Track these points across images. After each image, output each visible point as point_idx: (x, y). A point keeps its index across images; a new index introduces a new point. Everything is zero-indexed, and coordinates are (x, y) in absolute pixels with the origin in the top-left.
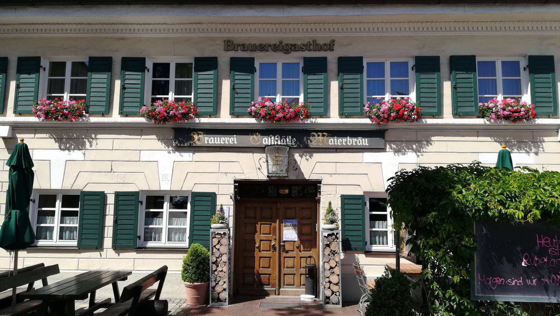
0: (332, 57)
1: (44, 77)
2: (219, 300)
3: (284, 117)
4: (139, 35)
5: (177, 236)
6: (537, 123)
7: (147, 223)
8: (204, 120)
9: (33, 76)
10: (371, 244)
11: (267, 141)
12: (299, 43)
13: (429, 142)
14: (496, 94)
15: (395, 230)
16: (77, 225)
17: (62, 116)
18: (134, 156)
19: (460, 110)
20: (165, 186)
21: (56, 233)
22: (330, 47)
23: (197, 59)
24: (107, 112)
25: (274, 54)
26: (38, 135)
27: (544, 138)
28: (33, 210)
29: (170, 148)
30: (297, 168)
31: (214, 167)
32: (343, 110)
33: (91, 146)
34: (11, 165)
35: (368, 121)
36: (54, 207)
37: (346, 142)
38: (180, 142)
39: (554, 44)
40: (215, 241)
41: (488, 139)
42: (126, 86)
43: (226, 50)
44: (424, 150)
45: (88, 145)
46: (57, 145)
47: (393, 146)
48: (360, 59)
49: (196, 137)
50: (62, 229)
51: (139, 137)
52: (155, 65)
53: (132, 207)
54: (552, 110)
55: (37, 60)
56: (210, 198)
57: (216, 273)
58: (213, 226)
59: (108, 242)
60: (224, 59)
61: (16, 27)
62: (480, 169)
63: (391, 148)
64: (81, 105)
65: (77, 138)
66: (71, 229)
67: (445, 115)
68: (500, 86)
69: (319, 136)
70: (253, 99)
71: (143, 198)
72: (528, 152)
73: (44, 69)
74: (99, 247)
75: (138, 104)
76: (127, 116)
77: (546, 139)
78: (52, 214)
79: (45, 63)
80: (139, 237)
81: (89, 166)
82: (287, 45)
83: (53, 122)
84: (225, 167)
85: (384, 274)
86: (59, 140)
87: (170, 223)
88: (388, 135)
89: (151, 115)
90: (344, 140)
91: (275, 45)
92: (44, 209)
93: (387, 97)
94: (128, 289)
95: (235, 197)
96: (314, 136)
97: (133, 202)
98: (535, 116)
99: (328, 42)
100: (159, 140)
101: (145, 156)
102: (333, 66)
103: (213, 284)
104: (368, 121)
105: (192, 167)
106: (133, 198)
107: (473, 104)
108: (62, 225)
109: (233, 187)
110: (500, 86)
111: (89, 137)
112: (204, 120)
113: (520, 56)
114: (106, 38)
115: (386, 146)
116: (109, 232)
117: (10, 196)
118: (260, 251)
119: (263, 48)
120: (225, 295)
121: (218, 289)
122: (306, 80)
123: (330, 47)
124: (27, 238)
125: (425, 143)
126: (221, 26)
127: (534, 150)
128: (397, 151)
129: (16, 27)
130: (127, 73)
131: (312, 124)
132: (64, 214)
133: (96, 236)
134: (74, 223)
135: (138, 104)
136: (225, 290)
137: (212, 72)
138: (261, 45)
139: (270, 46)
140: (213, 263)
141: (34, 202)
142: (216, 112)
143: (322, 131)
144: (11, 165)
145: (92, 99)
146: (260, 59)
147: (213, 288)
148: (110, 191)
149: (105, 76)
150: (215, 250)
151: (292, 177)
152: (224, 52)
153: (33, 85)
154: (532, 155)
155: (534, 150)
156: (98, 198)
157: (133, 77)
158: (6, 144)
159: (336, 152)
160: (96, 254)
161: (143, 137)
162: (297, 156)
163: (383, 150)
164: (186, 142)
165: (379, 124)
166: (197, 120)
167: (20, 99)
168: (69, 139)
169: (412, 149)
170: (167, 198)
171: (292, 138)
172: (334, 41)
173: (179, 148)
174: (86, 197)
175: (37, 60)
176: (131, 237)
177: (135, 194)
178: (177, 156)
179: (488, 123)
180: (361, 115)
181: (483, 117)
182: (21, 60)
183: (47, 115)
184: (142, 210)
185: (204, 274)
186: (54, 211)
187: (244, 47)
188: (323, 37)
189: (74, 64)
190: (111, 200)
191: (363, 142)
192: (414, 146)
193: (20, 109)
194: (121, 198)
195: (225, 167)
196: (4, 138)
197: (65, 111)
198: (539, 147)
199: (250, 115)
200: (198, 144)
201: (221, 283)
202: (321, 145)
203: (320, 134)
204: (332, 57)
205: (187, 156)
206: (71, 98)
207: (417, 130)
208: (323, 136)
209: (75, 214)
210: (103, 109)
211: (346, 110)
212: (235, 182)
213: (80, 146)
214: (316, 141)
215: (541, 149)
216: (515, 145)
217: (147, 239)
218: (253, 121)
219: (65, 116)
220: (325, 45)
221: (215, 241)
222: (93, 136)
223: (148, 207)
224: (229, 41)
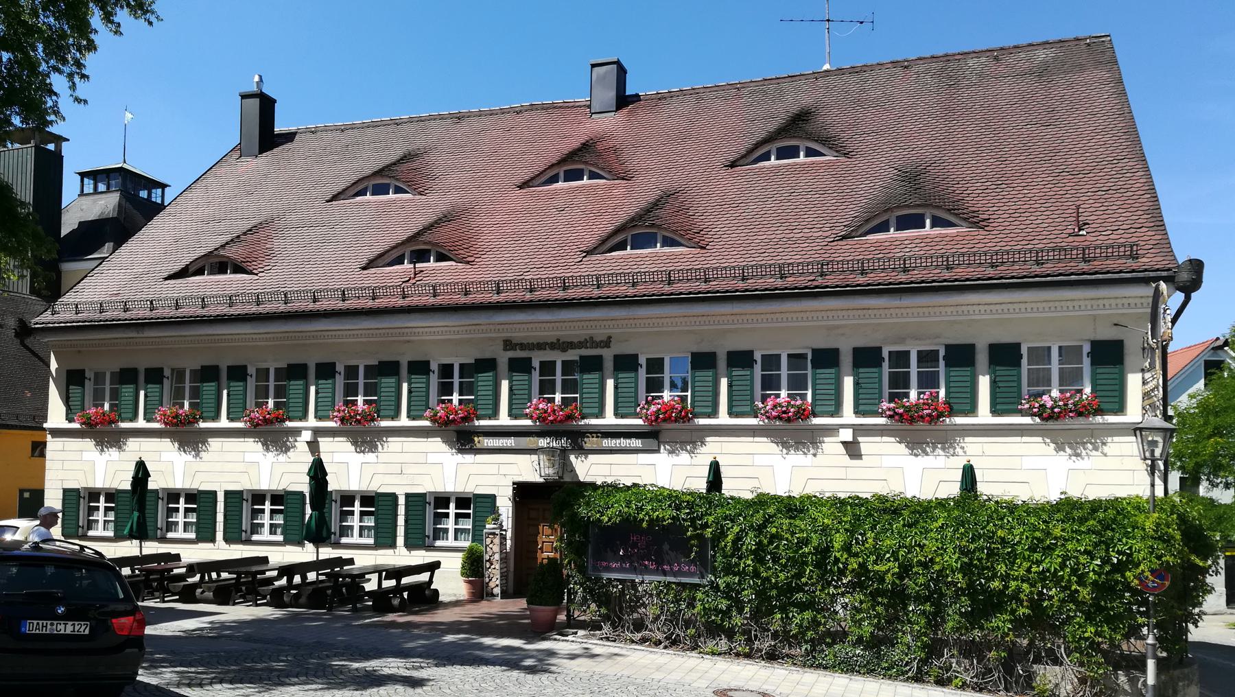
0: (608, 355)
1: (340, 381)
2: (493, 595)
3: (555, 420)
4: (423, 338)
5: (463, 536)
6: (813, 423)
7: (435, 524)
8: (483, 423)
9: (330, 381)
10: (167, 531)
11: (543, 442)
12: (576, 340)
13: (703, 443)
14: (909, 388)
16: (470, 527)
17: (355, 422)
18: (421, 459)
19: (861, 408)
20: (99, 484)
21: (451, 534)
22: (607, 343)
23: (816, 352)
24: (134, 417)
25: (552, 352)
26: (336, 439)
27: (825, 439)
28: (335, 510)
29: (454, 450)
30: (573, 470)
31: (494, 469)
32: (858, 408)
33: (383, 449)
35: (640, 422)
36: (179, 503)
37: (620, 444)
38: (462, 445)
39: (843, 334)
40: (489, 540)
41: (765, 439)
42: (412, 390)
43: (505, 349)
44: (698, 451)
45: (380, 446)
46: (907, 451)
47: (667, 447)
48: (1017, 346)
49: (476, 439)
50: (361, 528)
51: (425, 440)
52: (258, 370)
53: (420, 508)
54: (832, 408)
55: (332, 366)
56: (490, 500)
57: (490, 570)
58: (488, 526)
59: (400, 540)
60: (503, 358)
61: (313, 334)
63: (665, 449)
64: (373, 408)
65: (371, 442)
66: (369, 528)
67: (720, 415)
68: (784, 381)
69: (593, 437)
70: (530, 401)
71: (430, 499)
72: (805, 454)
73: (434, 372)
74: (213, 540)
75: (241, 410)
76: (622, 417)
77: (826, 439)
78: (352, 513)
79: (340, 368)
80: (428, 537)
81: (381, 468)
82: (564, 343)
83: (348, 427)
84: (504, 469)
85: (1206, 597)
86: (355, 443)
87: (271, 519)
88: (662, 437)
89: (433, 419)
90: (618, 441)
91: (552, 343)
92: (439, 511)
93: (558, 397)
95: (514, 499)
96: (588, 437)
97: (421, 503)
98: (696, 416)
99: (604, 338)
101: (432, 458)
102: (609, 365)
103: (487, 580)
104: (640, 422)
105: (474, 469)
106: (238, 496)
107: (749, 403)
108: (272, 522)
109: (511, 488)
110: (784, 381)
111: (380, 440)
112: (483, 423)
113: (1082, 340)
114: (394, 341)
115: (659, 447)
116: (401, 531)
118: (542, 552)
119: (540, 346)
120: (497, 591)
121: (492, 584)
122: (814, 375)
123: (607, 343)
124: (325, 534)
125: (699, 443)
126: (499, 327)
127: (812, 451)
128: (671, 452)
129: (313, 334)
130: (514, 374)
131: (586, 425)
132: (458, 516)
133: (390, 535)
134: (279, 520)
135: (424, 408)
136: (497, 586)
137: (491, 374)
138: (538, 344)
140: (487, 561)
141: (430, 504)
142: (495, 414)
143: (596, 433)
145: (479, 402)
146: (537, 359)
147: (488, 583)
148: (401, 492)
149: (393, 380)
150: (488, 549)
151: (567, 479)
153: (158, 394)
154: (810, 456)
155: (812, 451)
156: (390, 498)
157: (419, 380)
158: (846, 449)
159: (611, 454)
160: (390, 551)
161: (429, 439)
162: (572, 458)
163: (658, 451)
164: (468, 444)
165: (651, 425)
166: (477, 423)
167: (319, 404)
168: (364, 442)
169: (686, 450)
170: (183, 495)
171: (567, 439)
173: (461, 451)
174: (478, 500)
175: (332, 366)
176: (237, 530)
177: (423, 496)
178: (361, 457)
179: (761, 423)
180: (636, 416)
181: (756, 417)
182: (318, 366)
183: (342, 420)
184: (430, 511)
185: (478, 571)
186: (448, 513)
187: (523, 347)
188: (600, 333)
189: (366, 367)
190: (402, 501)
191: (636, 443)
192: (688, 448)
193: (319, 413)
195: (504, 469)
196: (307, 442)
197: (358, 417)
198: (818, 448)
199: (526, 416)
200: (479, 446)
201: (494, 580)
202: (595, 447)
203: (595, 435)
204: (608, 355)
205: (469, 458)
206: (366, 402)
207: (691, 430)
208: (597, 437)
209: (467, 516)
210: (392, 413)
211: (621, 411)
212: (514, 484)
213: (373, 448)
214: (590, 443)
215: (820, 450)
216: (792, 446)
217: (436, 538)
218: (528, 422)
219: (358, 422)
220: (602, 341)
221: (489, 540)
222: (384, 439)
223: (436, 508)
224: (507, 341)
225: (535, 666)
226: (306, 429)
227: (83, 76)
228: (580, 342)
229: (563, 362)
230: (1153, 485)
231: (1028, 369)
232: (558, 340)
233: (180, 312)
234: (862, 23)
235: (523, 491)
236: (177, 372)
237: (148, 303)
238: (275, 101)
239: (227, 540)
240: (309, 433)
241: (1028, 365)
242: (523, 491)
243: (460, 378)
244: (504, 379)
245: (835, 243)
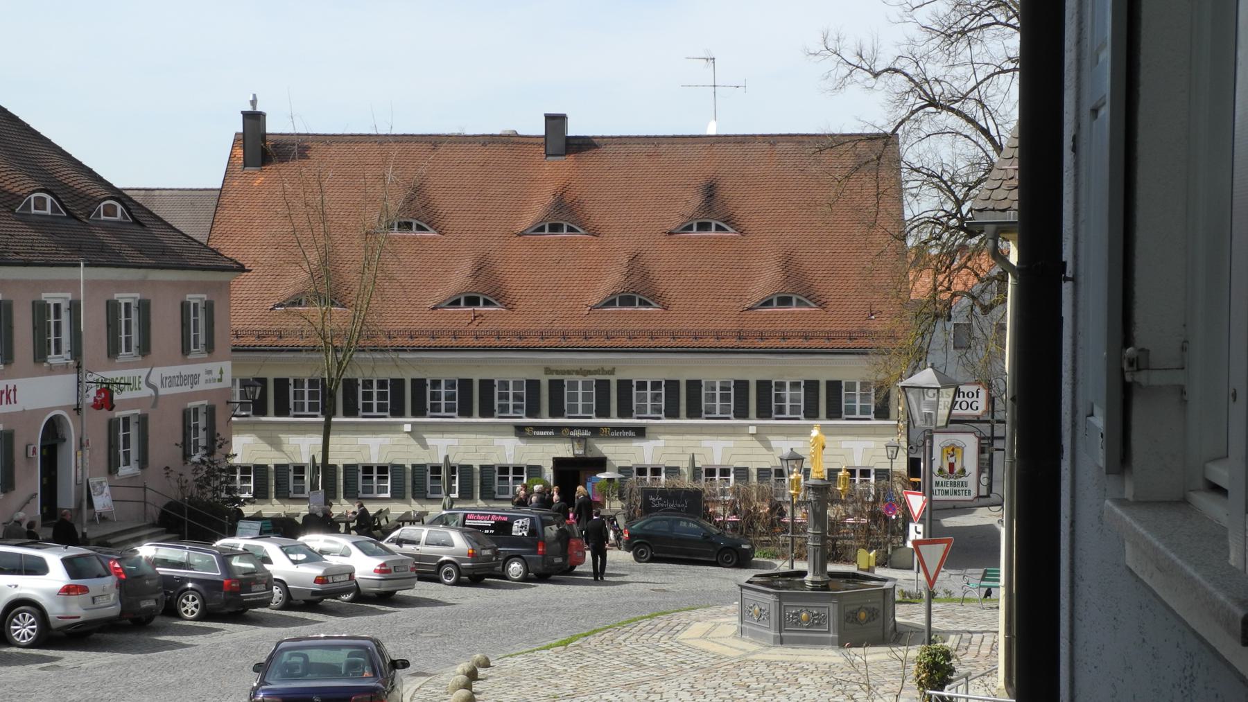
12: (593, 369)
15: (525, 535)
34: (343, 377)
43: (546, 374)
62: (145, 581)
82: (585, 370)
94: (362, 593)
99: (610, 369)
100: (269, 571)
117: (158, 532)
123: (612, 372)
139: (574, 371)
144: (343, 377)
148: (476, 465)
152: (545, 376)
172: (614, 369)
187: (558, 372)
188: (608, 367)
194: (879, 473)
220: (609, 371)
224: (547, 368)
225: (386, 663)
228: (595, 371)
229: (583, 382)
230: (931, 90)
232: (581, 369)
234: (738, 87)
235: (558, 462)
240: (410, 426)
242: (558, 462)
243: (304, 403)
244: (4, 426)
245: (744, 313)
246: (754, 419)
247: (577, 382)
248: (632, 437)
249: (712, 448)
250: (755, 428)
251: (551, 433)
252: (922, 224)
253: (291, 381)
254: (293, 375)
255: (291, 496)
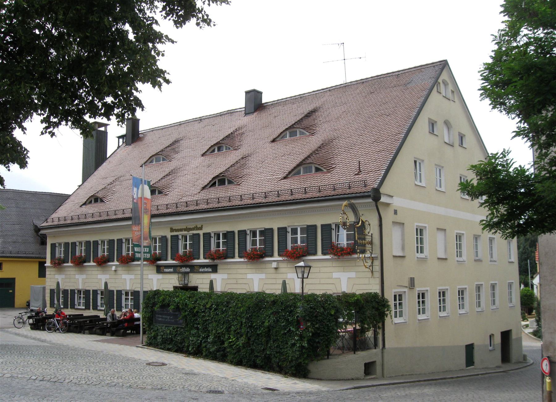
123: (201, 228)
139: (183, 229)
152: (170, 233)
211: (281, 253)
226: (274, 261)
227: (31, 121)
228: (193, 228)
231: (291, 237)
233: (308, 196)
236: (217, 234)
237: (240, 196)
238: (261, 93)
239: (93, 309)
241: (292, 235)
246: (237, 259)
247: (297, 229)
248: (210, 272)
249: (252, 279)
250: (276, 263)
251: (172, 270)
252: (187, 123)
253: (289, 230)
254: (124, 237)
255: (98, 309)
